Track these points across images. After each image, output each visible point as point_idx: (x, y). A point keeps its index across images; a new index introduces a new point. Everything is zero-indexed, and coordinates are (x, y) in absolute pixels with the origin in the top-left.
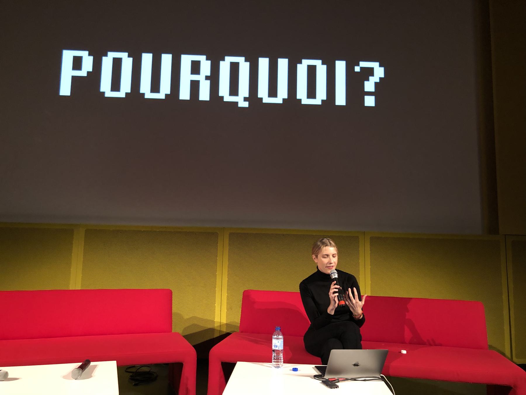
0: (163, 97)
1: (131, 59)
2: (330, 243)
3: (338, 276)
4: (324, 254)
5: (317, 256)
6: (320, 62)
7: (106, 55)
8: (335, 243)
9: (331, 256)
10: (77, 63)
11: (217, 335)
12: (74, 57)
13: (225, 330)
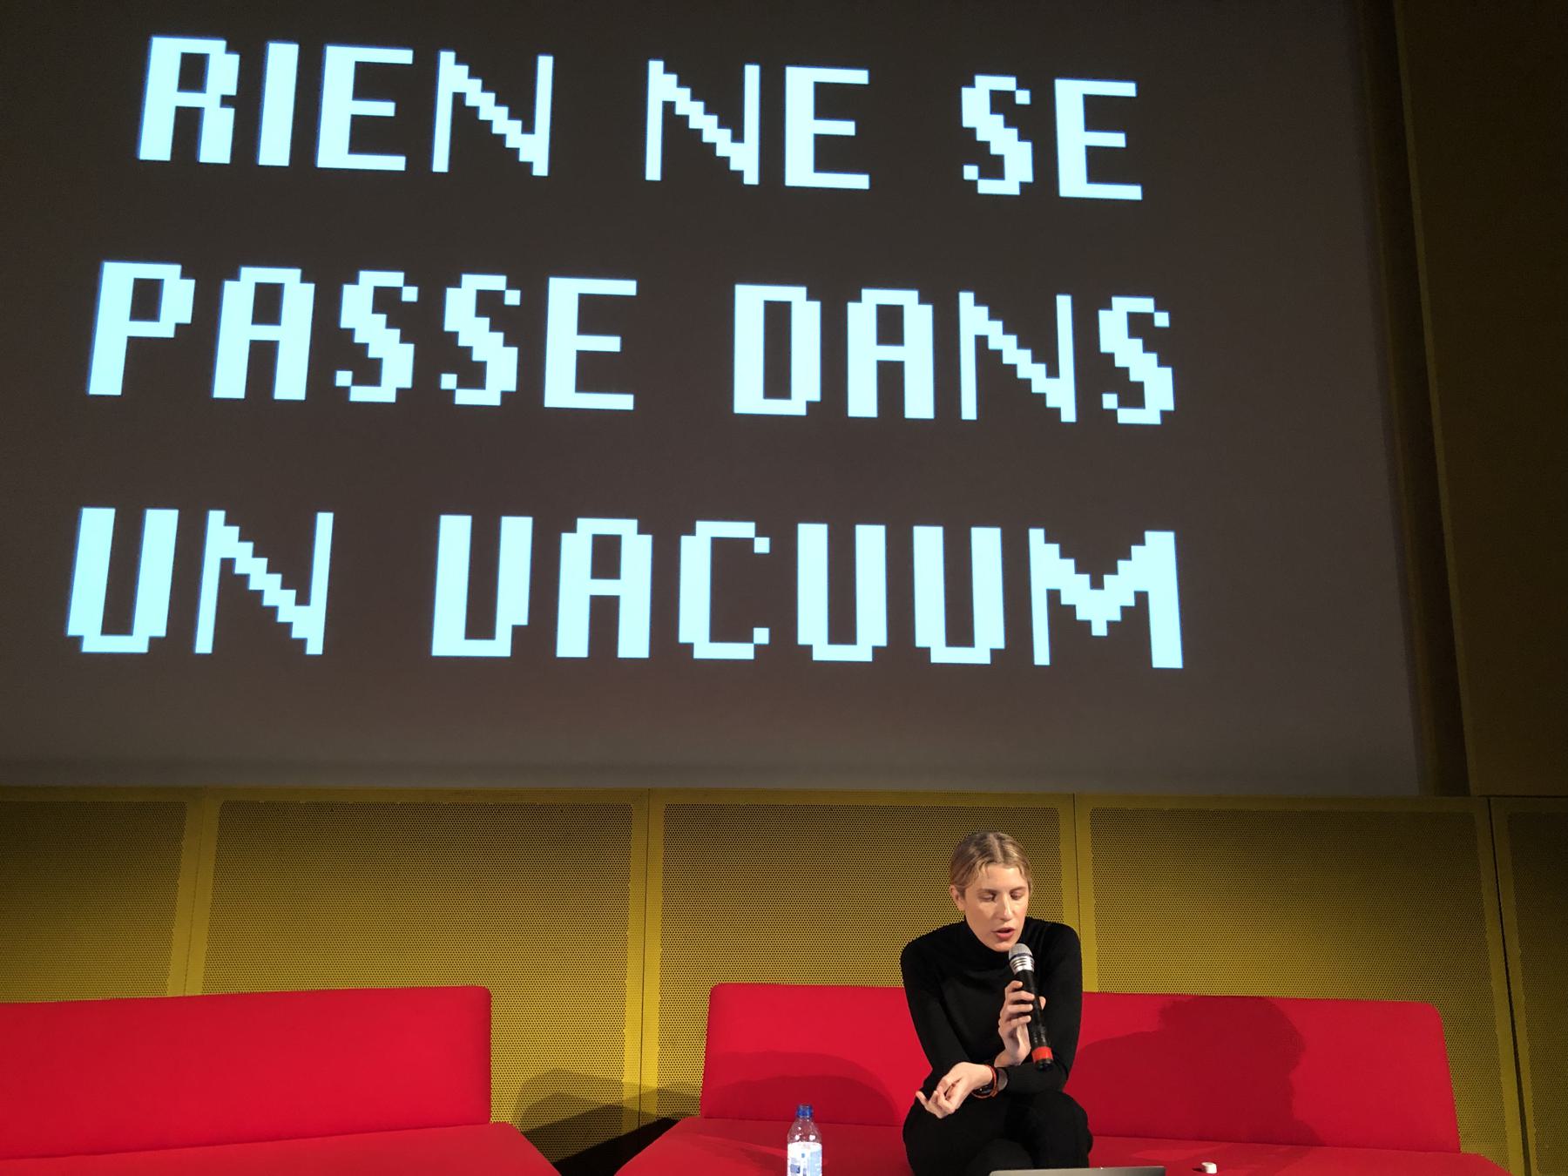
0: (495, 401)
1: (310, 288)
2: (1005, 854)
3: (1035, 965)
4: (985, 886)
5: (962, 893)
6: (801, 291)
7: (457, 284)
8: (1020, 851)
9: (1006, 897)
10: (146, 300)
11: (628, 1127)
12: (258, 285)
13: (653, 1110)
